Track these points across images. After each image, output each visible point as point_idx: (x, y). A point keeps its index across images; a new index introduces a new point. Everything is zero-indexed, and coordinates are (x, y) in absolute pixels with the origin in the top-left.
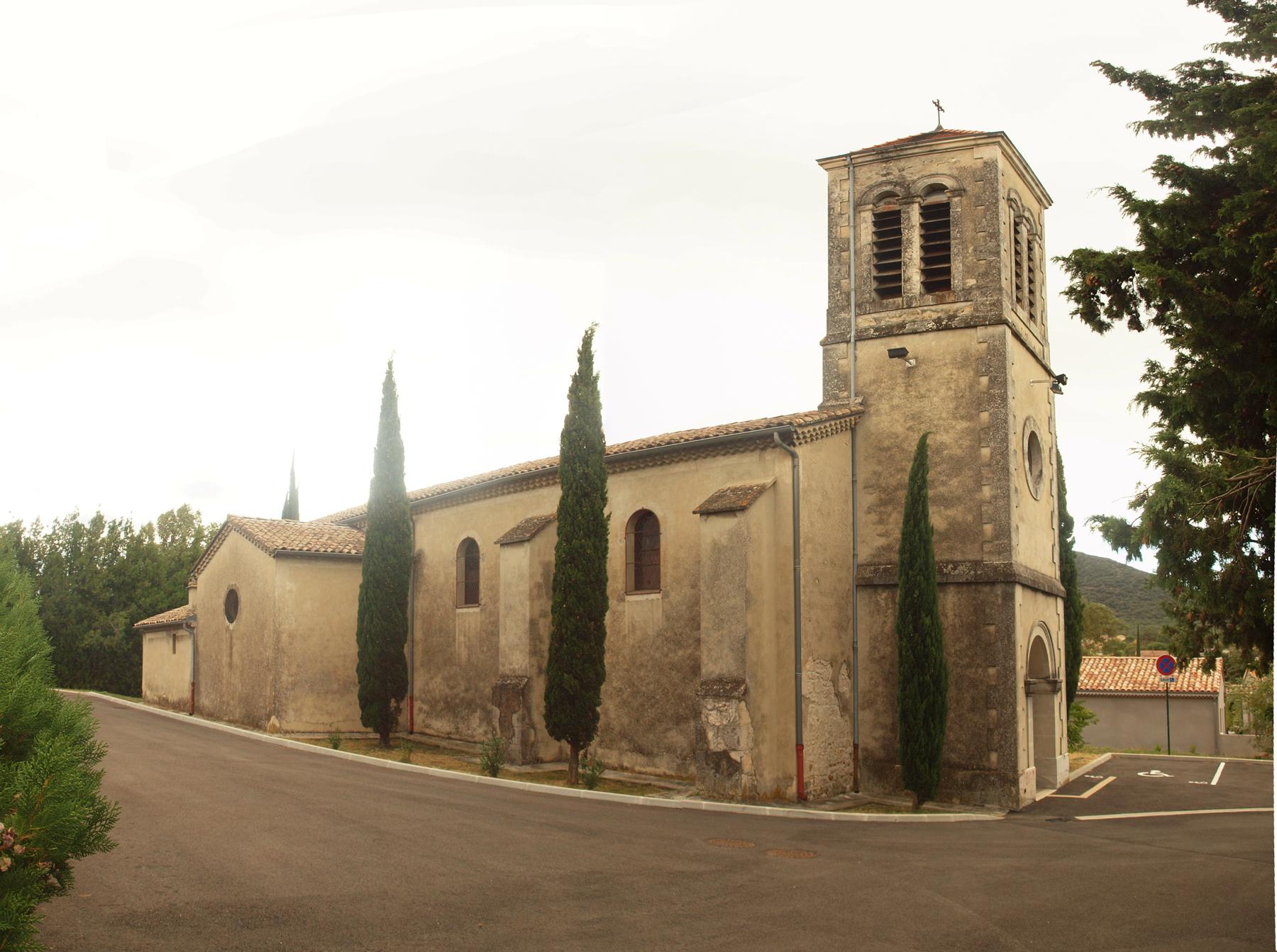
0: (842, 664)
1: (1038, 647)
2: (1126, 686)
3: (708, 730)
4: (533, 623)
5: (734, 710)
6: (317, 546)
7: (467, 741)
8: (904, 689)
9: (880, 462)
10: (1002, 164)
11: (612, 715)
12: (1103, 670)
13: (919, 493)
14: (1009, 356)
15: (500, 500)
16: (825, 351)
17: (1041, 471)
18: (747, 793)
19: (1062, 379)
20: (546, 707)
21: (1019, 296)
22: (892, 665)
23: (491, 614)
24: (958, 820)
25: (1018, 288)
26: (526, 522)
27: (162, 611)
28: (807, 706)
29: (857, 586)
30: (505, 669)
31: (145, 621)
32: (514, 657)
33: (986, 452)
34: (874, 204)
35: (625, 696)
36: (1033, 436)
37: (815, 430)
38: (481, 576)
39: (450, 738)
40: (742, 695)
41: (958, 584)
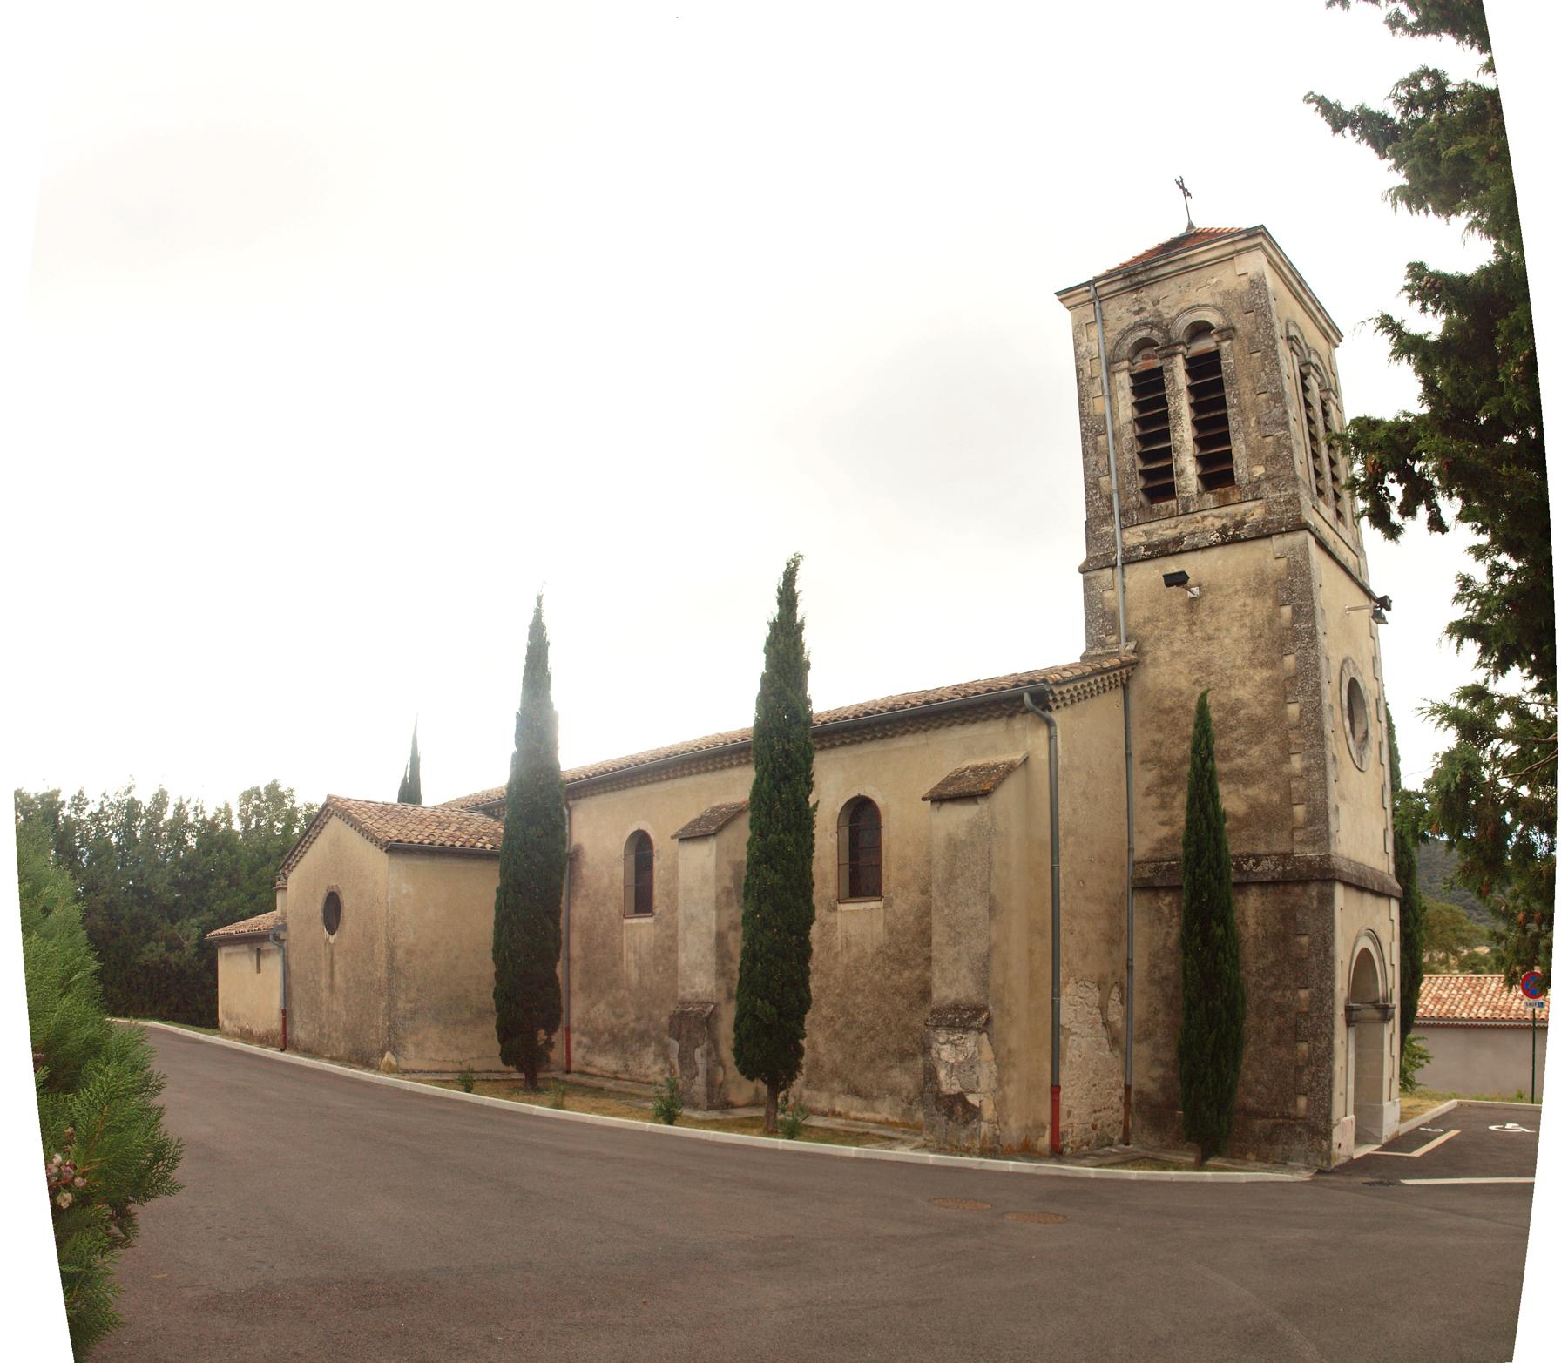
0: (1112, 986)
1: (1364, 963)
2: (1482, 1012)
3: (939, 1068)
4: (720, 937)
5: (973, 1044)
6: (442, 838)
7: (639, 1082)
8: (1189, 1017)
9: (1160, 729)
10: (1272, 281)
11: (822, 1049)
12: (1454, 992)
13: (1203, 767)
14: (1314, 575)
15: (679, 783)
16: (1086, 581)
17: (1366, 732)
18: (988, 1146)
19: (1384, 603)
20: (735, 1040)
21: (1320, 487)
22: (1176, 987)
23: (668, 926)
24: (1250, 1180)
25: (1318, 474)
26: (711, 811)
27: (242, 918)
28: (1067, 1038)
29: (1133, 889)
30: (685, 993)
31: (220, 931)
32: (697, 979)
33: (1293, 709)
34: (1130, 360)
35: (837, 1027)
36: (1353, 684)
37: (1075, 688)
38: (655, 879)
39: (617, 1078)
40: (984, 1025)
41: (1261, 884)
